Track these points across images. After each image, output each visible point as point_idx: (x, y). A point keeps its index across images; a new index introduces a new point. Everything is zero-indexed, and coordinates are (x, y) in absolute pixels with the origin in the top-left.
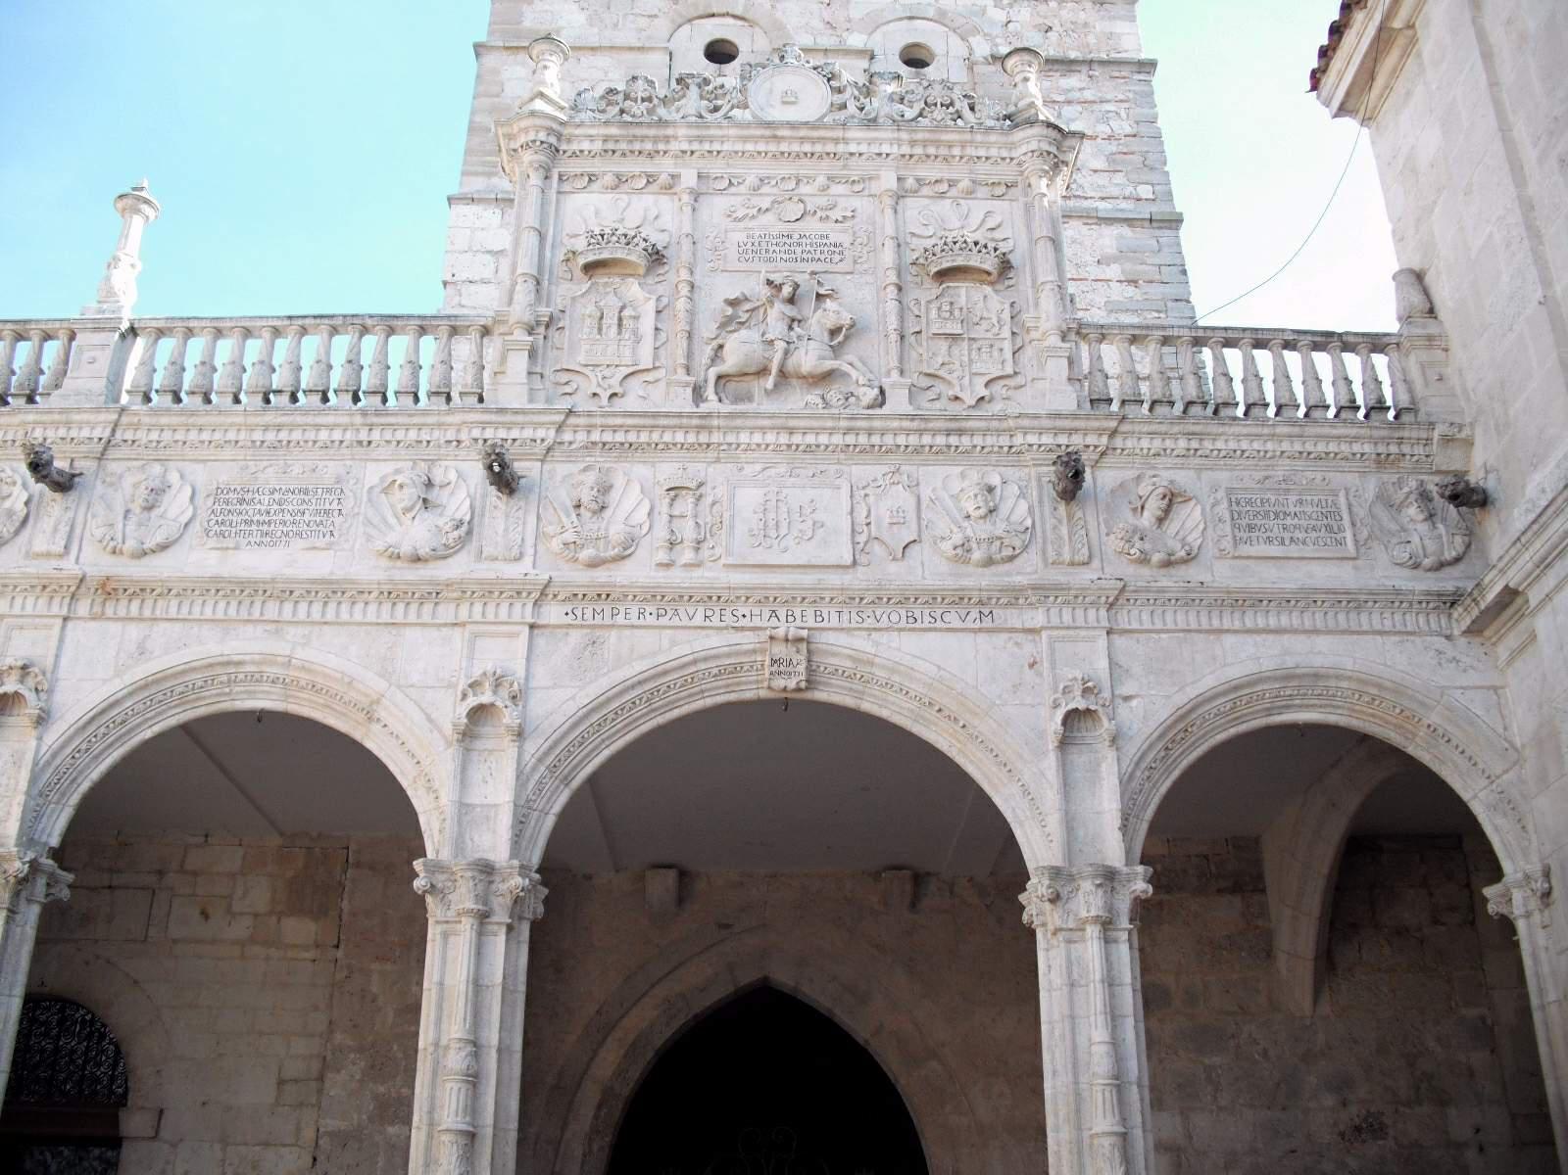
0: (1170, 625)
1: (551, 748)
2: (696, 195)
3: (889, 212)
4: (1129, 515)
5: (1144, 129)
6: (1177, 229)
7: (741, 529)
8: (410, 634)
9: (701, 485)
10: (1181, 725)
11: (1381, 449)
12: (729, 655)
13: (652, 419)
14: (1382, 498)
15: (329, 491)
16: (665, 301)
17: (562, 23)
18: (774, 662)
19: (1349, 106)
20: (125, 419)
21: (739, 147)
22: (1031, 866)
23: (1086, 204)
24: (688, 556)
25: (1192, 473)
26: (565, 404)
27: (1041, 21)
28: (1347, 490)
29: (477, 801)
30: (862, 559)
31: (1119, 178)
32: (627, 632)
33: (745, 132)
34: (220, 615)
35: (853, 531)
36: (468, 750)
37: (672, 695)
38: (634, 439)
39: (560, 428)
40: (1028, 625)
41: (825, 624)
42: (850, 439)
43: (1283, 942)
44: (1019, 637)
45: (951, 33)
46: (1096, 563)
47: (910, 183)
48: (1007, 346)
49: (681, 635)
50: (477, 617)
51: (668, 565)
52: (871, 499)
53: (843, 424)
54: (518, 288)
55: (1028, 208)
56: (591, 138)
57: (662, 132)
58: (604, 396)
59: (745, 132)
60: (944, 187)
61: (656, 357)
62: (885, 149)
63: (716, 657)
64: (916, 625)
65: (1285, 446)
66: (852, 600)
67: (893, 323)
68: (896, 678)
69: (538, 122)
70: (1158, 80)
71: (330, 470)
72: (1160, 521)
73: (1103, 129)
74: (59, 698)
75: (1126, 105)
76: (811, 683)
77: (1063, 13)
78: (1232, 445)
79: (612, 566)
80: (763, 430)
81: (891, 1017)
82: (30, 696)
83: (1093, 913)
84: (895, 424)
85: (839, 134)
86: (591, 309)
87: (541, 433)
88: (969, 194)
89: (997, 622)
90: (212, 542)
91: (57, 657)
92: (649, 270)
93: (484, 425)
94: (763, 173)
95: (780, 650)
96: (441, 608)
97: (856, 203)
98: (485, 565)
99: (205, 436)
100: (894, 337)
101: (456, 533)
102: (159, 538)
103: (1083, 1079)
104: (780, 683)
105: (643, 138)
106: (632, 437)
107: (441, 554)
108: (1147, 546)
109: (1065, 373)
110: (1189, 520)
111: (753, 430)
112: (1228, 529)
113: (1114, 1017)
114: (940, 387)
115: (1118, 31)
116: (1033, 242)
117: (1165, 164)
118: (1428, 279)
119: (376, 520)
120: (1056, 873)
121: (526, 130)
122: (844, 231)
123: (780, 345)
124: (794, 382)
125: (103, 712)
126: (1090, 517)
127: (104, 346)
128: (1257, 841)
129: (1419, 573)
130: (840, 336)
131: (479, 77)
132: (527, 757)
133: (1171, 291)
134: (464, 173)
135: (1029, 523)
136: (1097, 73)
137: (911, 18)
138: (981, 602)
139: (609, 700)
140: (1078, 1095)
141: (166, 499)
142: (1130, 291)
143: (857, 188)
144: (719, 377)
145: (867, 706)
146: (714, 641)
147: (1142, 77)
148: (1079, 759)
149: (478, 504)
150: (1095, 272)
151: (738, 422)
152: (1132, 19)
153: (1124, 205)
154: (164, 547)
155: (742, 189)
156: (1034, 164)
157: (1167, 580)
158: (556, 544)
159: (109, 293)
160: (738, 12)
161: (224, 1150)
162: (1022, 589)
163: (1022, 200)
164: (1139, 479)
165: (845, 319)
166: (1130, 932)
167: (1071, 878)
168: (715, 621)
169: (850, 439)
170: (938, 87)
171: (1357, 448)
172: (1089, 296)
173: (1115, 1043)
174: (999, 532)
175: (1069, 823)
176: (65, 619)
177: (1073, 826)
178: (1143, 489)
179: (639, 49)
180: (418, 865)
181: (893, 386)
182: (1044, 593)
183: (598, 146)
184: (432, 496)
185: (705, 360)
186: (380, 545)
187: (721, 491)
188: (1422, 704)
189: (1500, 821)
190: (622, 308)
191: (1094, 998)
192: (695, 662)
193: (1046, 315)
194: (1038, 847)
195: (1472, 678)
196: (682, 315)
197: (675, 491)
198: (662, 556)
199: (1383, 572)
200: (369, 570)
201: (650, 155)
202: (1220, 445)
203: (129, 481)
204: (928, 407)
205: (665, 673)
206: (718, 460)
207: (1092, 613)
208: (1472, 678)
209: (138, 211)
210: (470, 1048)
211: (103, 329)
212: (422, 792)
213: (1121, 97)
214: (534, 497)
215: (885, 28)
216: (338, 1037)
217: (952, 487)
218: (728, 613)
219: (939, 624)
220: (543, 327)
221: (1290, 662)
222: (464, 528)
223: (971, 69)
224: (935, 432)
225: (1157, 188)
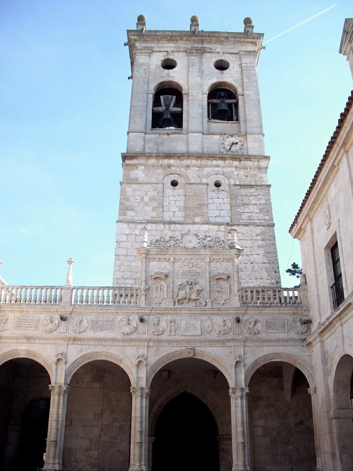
0: (255, 345)
1: (151, 368)
2: (173, 263)
3: (208, 266)
4: (249, 325)
5: (268, 202)
6: (274, 227)
7: (182, 328)
8: (127, 347)
9: (175, 320)
10: (256, 362)
11: (294, 312)
12: (180, 351)
13: (167, 309)
14: (294, 321)
15: (111, 321)
16: (168, 284)
17: (139, 176)
18: (188, 352)
19: (296, 237)
20: (75, 308)
21: (181, 253)
22: (230, 387)
23: (254, 221)
24: (173, 334)
25: (260, 317)
26: (152, 307)
27: (246, 174)
28: (287, 319)
29: (140, 376)
30: (203, 334)
31: (262, 215)
32: (163, 347)
33: (182, 250)
34: (94, 344)
35: (201, 329)
36: (138, 368)
37: (171, 358)
38: (165, 312)
39: (151, 310)
40: (230, 345)
41: (196, 346)
42: (201, 312)
43: (285, 387)
44: (229, 348)
45: (225, 178)
46: (242, 334)
47: (212, 259)
48: (228, 293)
49: (173, 348)
50: (138, 344)
51: (170, 335)
52: (204, 323)
53: (199, 309)
54: (142, 283)
55: (233, 265)
56: (154, 251)
57: (167, 250)
58: (158, 303)
59: (182, 250)
60: (218, 260)
61: (167, 296)
62: (208, 253)
63: (178, 351)
64: (212, 346)
65: (277, 312)
66: (201, 341)
67: (208, 289)
68: (208, 355)
69: (145, 249)
70: (271, 189)
71: (111, 317)
72: (254, 326)
73: (259, 202)
74: (68, 358)
75: (264, 196)
76: (194, 355)
77: (251, 172)
78: (267, 312)
79: (161, 335)
80: (186, 310)
81: (210, 399)
82: (63, 358)
83: (239, 395)
84: (208, 309)
85: (199, 250)
86: (155, 286)
87: (148, 311)
88: (223, 261)
89: (225, 345)
90: (92, 331)
91: (67, 351)
92: (165, 278)
93: (138, 310)
94: (186, 258)
95: (189, 350)
96: (132, 343)
97: (202, 263)
98: (139, 335)
99: (89, 311)
100: (208, 292)
101: (134, 330)
102: (83, 330)
103: (237, 422)
104: (189, 356)
105: (164, 251)
106: (163, 312)
107: (132, 333)
108: (251, 331)
109: (238, 299)
110: (259, 325)
111: (184, 310)
112: (265, 327)
113: (242, 412)
114: (216, 301)
115: (263, 176)
116: (234, 272)
117: (272, 210)
118: (306, 276)
119: (120, 326)
120: (233, 389)
121: (142, 250)
122: (200, 270)
123: (189, 294)
124: (191, 300)
125: (76, 361)
126: (241, 325)
127: (69, 292)
128: (281, 367)
129: (299, 335)
130: (199, 292)
131: (121, 190)
132: (148, 369)
133: (271, 242)
134: (119, 215)
135: (231, 327)
136: (258, 188)
137: (217, 174)
138: (222, 342)
139: (161, 359)
140: (236, 424)
141: (83, 322)
142: (263, 242)
143: (202, 260)
144: (178, 300)
145: (204, 359)
146: (178, 349)
147: (268, 189)
148: (238, 369)
149: (137, 324)
150: (255, 238)
151: (181, 309)
152: (266, 173)
153: (262, 221)
154: (83, 332)
155: (182, 261)
156: (234, 256)
157: (254, 338)
158: (151, 331)
159: (68, 281)
160: (178, 173)
161: (84, 428)
162: (229, 339)
163: (232, 262)
164: (250, 318)
165: (200, 289)
166: (246, 398)
167: (236, 389)
168: (178, 345)
169: (201, 312)
170: (217, 238)
171: (289, 312)
172: (254, 244)
173: (242, 417)
174: (226, 329)
175: (236, 380)
176: (68, 344)
177: (237, 379)
178: (251, 320)
179: (157, 183)
180: (131, 388)
181: (209, 302)
182: (233, 340)
183: (155, 253)
184: (130, 322)
185: (176, 297)
186: (121, 332)
187: (179, 322)
188: (297, 358)
189: (310, 378)
190: (161, 286)
191: (239, 409)
192: (175, 352)
193: (235, 287)
194: (231, 384)
195: (307, 354)
196: (171, 288)
197: (171, 322)
198: (169, 334)
199: (293, 335)
200: (119, 336)
201: (165, 255)
202: (265, 312)
203: (76, 318)
204: (215, 306)
205: (170, 354)
206: (178, 316)
207: (241, 343)
208: (307, 354)
209: (71, 264)
210: (141, 418)
211: (68, 289)
212: (130, 374)
213: (263, 194)
214: (147, 323)
215: (211, 177)
216: (105, 406)
217: (218, 320)
218: (180, 343)
219: (215, 345)
220: (147, 290)
221: (275, 351)
222: (135, 328)
223: (230, 187)
224: (215, 311)
225: (270, 217)
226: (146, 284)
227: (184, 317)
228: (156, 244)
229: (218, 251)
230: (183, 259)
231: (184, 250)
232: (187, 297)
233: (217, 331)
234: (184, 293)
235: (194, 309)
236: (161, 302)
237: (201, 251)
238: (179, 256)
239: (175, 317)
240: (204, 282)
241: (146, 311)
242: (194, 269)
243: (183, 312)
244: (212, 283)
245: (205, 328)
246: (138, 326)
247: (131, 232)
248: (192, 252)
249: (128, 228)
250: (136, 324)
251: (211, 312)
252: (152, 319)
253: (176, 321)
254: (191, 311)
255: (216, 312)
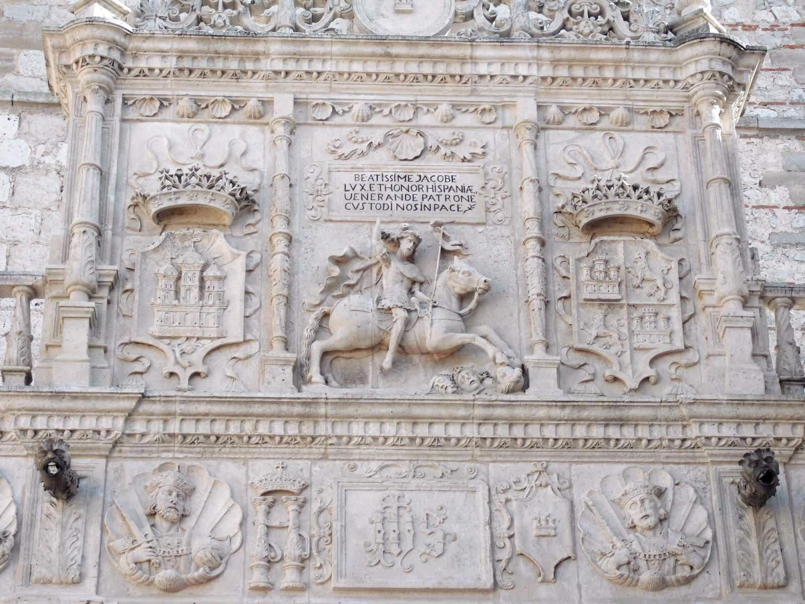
2: (293, 126)
3: (528, 148)
7: (353, 542)
9: (305, 487)
13: (244, 406)
16: (256, 257)
21: (344, 67)
24: (289, 577)
26: (134, 387)
30: (505, 580)
33: (354, 49)
35: (493, 545)
39: (130, 416)
42: (487, 431)
47: (553, 111)
48: (676, 314)
52: (514, 505)
53: (479, 412)
54: (75, 240)
55: (697, 142)
56: (163, 54)
58: (184, 376)
59: (354, 49)
60: (594, 117)
61: (246, 328)
62: (522, 70)
67: (535, 286)
69: (98, 32)
80: (380, 419)
84: (542, 412)
85: (467, 51)
86: (165, 267)
87: (105, 423)
88: (625, 125)
93: (34, 413)
94: (373, 98)
100: (537, 303)
105: (227, 55)
106: (219, 428)
111: (368, 419)
114: (595, 366)
116: (704, 185)
121: (82, 42)
124: (416, 358)
130: (471, 303)
135: (708, 534)
143: (488, 118)
144: (325, 354)
149: (25, 512)
151: (350, 410)
153: (792, 112)
155: (348, 119)
156: (703, 89)
158: (125, 563)
163: (690, 132)
169: (487, 431)
174: (673, 547)
181: (538, 365)
183: (171, 63)
185: (307, 333)
187: (330, 496)
193: (722, 277)
196: (278, 276)
197: (272, 496)
198: (258, 578)
201: (236, 76)
206: (325, 457)
214: (97, 504)
217: (612, 489)
220: (108, 288)
224: (590, 422)
226: (101, 255)
227: (363, 469)
228: (176, 19)
229: (594, 55)
230: (359, 108)
231: (369, 49)
232: (388, 332)
233: (608, 564)
234: (371, 304)
235: (443, 412)
236: (201, 369)
237: (479, 52)
238: (331, 90)
239: (300, 467)
240: (503, 250)
241: (90, 423)
242: (434, 166)
243: (357, 429)
244: (559, 250)
245: (524, 540)
246: (32, 525)
247: (38, 156)
248: (422, 58)
249: (19, 136)
250: (12, 510)
251: (564, 432)
252: (129, 481)
253: (312, 493)
254: (415, 421)
255: (597, 432)
